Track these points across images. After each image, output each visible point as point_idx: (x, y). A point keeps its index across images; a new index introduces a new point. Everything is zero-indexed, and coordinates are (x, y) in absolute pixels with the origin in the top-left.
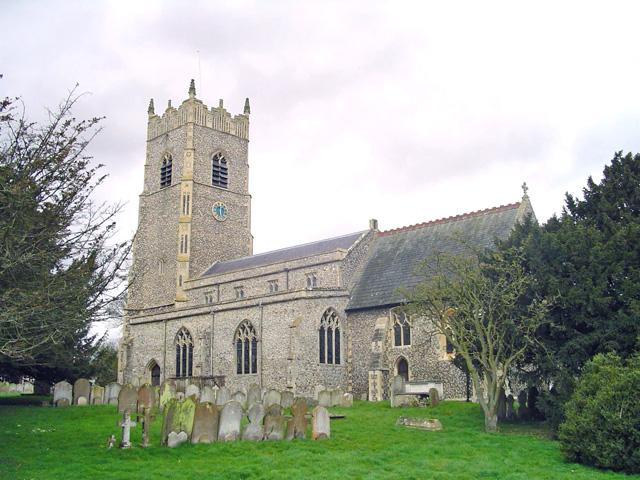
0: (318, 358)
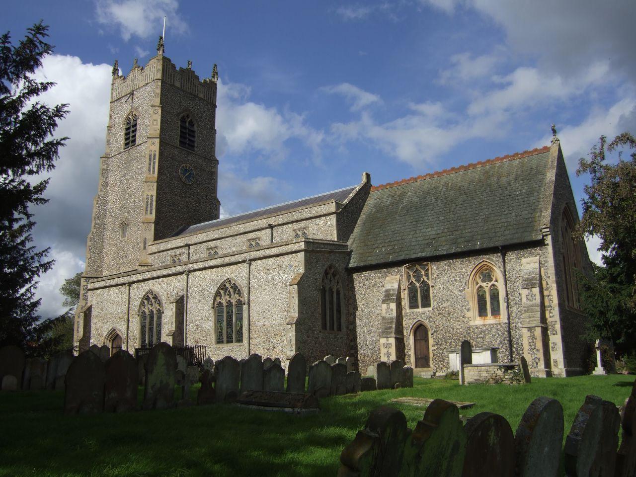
0: (320, 323)
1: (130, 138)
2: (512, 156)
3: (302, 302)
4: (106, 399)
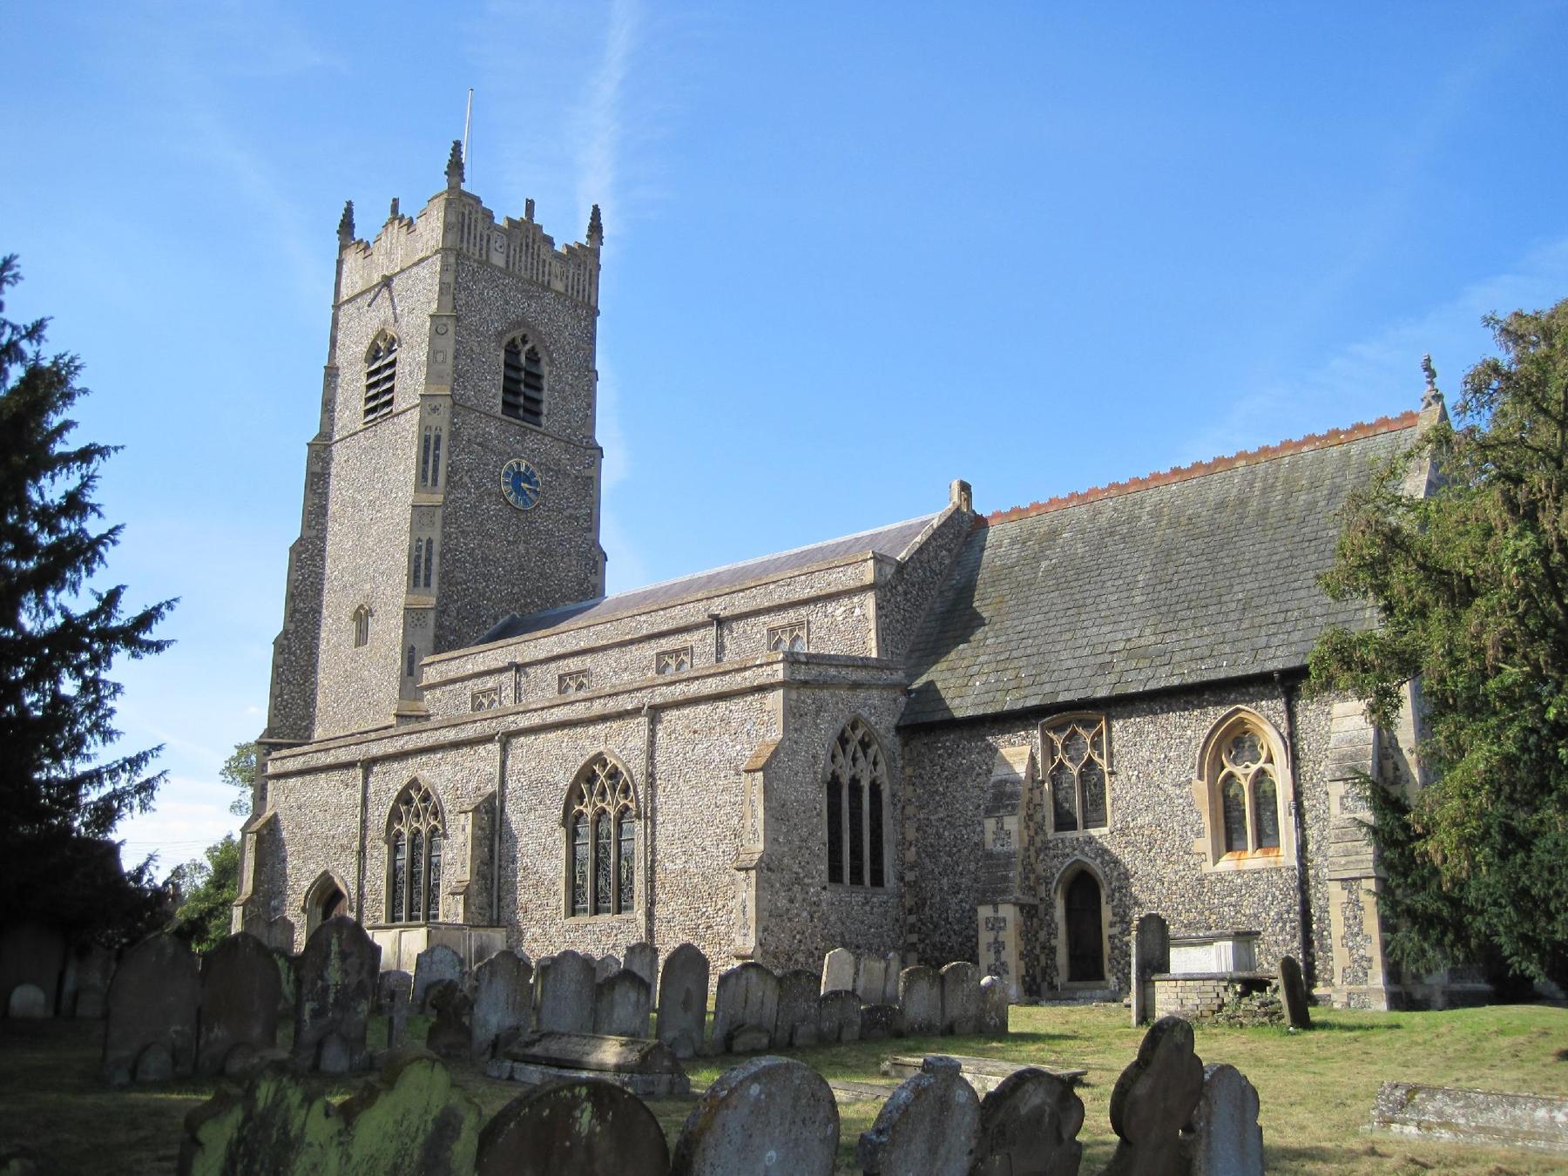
1: (379, 400)
2: (1324, 437)
3: (777, 813)
4: (202, 1042)
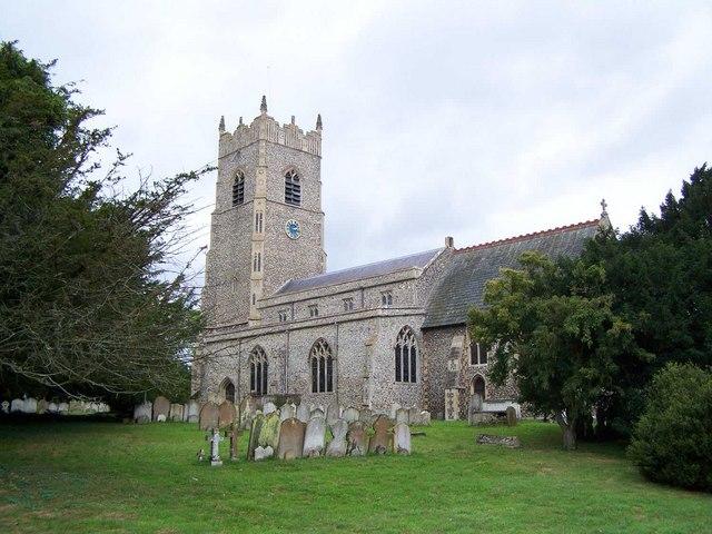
0: (394, 376)
